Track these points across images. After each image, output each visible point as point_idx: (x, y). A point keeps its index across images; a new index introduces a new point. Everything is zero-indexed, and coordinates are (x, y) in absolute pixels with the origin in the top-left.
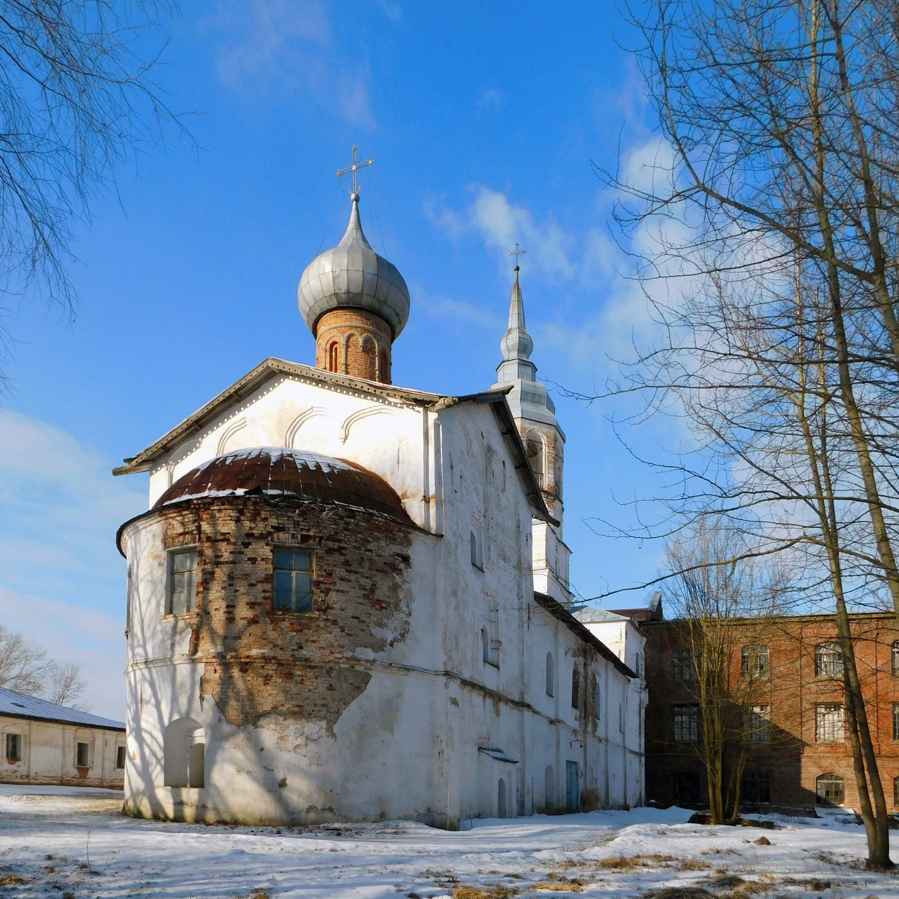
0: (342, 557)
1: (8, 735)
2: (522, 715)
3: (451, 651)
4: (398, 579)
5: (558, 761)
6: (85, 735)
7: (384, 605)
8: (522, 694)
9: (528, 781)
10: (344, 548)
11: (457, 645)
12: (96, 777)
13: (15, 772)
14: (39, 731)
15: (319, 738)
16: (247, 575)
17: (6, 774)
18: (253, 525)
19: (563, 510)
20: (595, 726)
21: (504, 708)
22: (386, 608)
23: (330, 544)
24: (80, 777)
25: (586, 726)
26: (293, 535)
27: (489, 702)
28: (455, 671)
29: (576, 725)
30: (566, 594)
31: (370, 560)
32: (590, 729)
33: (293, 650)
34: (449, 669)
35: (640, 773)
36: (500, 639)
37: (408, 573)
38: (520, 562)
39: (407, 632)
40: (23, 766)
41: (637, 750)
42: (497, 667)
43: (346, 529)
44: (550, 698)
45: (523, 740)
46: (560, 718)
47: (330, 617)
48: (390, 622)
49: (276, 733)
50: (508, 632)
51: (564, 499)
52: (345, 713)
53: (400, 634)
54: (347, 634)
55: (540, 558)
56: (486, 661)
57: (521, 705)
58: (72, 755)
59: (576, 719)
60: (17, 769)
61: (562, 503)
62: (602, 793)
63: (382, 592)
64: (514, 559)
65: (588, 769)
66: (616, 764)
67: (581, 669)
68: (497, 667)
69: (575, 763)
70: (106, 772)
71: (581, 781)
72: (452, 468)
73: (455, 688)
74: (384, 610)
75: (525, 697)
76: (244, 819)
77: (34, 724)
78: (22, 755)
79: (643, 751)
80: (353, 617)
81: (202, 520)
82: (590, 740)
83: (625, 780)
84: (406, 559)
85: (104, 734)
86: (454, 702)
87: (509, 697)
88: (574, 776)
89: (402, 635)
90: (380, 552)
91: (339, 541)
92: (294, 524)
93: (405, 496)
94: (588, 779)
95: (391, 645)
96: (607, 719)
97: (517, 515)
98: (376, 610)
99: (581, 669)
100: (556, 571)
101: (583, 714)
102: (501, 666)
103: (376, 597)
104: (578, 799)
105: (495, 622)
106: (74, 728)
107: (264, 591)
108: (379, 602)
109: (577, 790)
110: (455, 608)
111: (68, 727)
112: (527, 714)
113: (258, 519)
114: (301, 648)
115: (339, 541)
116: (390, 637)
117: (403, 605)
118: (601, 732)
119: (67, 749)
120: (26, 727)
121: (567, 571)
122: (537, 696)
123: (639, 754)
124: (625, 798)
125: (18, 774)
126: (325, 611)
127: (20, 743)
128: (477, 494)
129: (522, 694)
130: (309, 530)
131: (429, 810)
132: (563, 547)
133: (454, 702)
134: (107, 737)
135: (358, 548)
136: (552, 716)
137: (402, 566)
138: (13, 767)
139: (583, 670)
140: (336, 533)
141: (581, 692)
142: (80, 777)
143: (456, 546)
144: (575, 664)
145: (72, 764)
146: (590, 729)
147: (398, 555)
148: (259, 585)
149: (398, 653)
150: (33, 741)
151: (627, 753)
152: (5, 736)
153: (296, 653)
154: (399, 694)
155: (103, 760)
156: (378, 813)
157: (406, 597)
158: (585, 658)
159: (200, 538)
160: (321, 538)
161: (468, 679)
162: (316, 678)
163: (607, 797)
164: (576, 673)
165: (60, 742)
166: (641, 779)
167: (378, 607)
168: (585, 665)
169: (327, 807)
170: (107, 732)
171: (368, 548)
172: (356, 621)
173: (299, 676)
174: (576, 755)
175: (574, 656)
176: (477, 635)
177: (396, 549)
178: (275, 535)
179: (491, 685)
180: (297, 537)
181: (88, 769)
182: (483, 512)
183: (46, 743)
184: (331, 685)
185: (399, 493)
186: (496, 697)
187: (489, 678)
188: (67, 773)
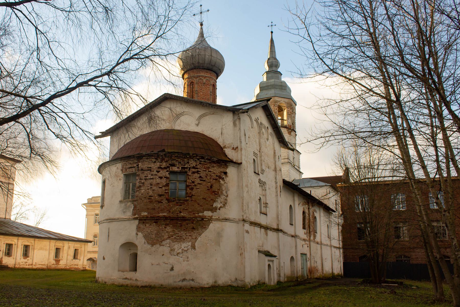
0: (198, 175)
1: (24, 245)
2: (278, 235)
3: (245, 210)
4: (222, 182)
5: (296, 254)
6: (59, 244)
7: (216, 193)
8: (278, 225)
9: (282, 264)
10: (200, 171)
11: (248, 207)
12: (64, 264)
13: (26, 262)
14: (38, 244)
15: (188, 249)
16: (159, 184)
17: (22, 264)
18: (161, 164)
19: (296, 135)
20: (315, 237)
21: (269, 232)
22: (217, 194)
23: (194, 170)
24: (56, 264)
25: (310, 237)
26: (178, 168)
27: (263, 230)
28: (247, 218)
29: (305, 237)
30: (298, 173)
31: (211, 175)
32: (312, 238)
33: (178, 213)
34: (244, 218)
35: (340, 257)
36: (267, 202)
37: (227, 180)
38: (275, 168)
39: (226, 203)
40: (30, 259)
41: (338, 246)
42: (266, 215)
43: (200, 164)
44: (291, 226)
45: (279, 246)
46: (297, 234)
47: (193, 199)
48: (219, 200)
49: (169, 248)
50: (271, 198)
51: (297, 130)
52: (199, 239)
53: (223, 205)
54: (200, 206)
55: (285, 158)
56: (261, 213)
57: (278, 230)
58: (53, 253)
59: (305, 234)
60: (27, 261)
61: (295, 132)
62: (320, 268)
63: (215, 188)
64: (273, 167)
65: (312, 257)
66: (327, 252)
67: (307, 211)
68: (266, 215)
69: (306, 254)
70: (68, 261)
71: (308, 263)
72: (245, 135)
73: (247, 227)
74: (216, 195)
75: (280, 227)
76: (154, 285)
77: (37, 240)
78: (30, 255)
79: (341, 246)
80: (203, 199)
81: (139, 162)
82: (312, 244)
83: (332, 261)
84: (226, 173)
85: (68, 243)
86: (247, 232)
87: (272, 227)
88: (305, 261)
89: (224, 205)
90: (214, 172)
91: (197, 168)
92: (179, 163)
93: (225, 147)
94: (312, 261)
95: (219, 209)
96: (321, 233)
97: (274, 148)
98: (213, 195)
99: (307, 211)
100: (293, 163)
101: (308, 231)
102: (268, 214)
103: (213, 190)
104: (307, 271)
105: (265, 195)
106: (55, 241)
107: (166, 190)
108: (214, 192)
109: (307, 267)
110: (247, 192)
111: (52, 241)
112: (281, 234)
113: (163, 161)
114: (181, 212)
115: (197, 168)
116: (219, 206)
117: (224, 192)
118: (318, 239)
119: (51, 251)
120: (33, 242)
121: (299, 162)
122: (285, 225)
123: (339, 248)
124: (333, 270)
125: (27, 264)
126: (191, 197)
127: (29, 249)
128: (256, 143)
129: (278, 225)
130: (185, 165)
131: (236, 279)
132: (297, 152)
133: (247, 232)
134: (70, 245)
135: (205, 171)
136: (293, 234)
137: (224, 176)
138: (26, 260)
139: (307, 211)
140: (196, 166)
141: (307, 221)
142: (56, 264)
143: (247, 167)
144: (303, 209)
145: (52, 258)
146: (312, 238)
147: (222, 172)
148: (163, 187)
149: (222, 213)
150: (35, 248)
151: (333, 248)
152: (23, 246)
153: (178, 214)
154: (223, 230)
155: (67, 256)
156: (214, 281)
157: (226, 189)
158: (309, 205)
159: (138, 170)
160: (190, 168)
161: (253, 221)
162: (187, 224)
163: (322, 270)
164: (304, 213)
165: (48, 248)
166: (340, 259)
167: (214, 194)
168: (309, 208)
169: (191, 279)
170: (70, 242)
171: (209, 170)
172: (204, 200)
173: (180, 224)
174: (306, 250)
175: (303, 205)
176: (257, 202)
177: (222, 170)
178: (171, 168)
179: (263, 223)
180: (179, 168)
181: (60, 260)
182: (259, 150)
183: (41, 249)
184: (193, 227)
185: (222, 146)
186: (266, 228)
187: (263, 220)
188: (50, 262)
